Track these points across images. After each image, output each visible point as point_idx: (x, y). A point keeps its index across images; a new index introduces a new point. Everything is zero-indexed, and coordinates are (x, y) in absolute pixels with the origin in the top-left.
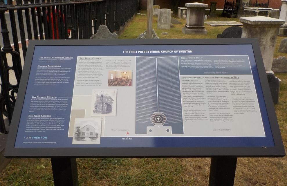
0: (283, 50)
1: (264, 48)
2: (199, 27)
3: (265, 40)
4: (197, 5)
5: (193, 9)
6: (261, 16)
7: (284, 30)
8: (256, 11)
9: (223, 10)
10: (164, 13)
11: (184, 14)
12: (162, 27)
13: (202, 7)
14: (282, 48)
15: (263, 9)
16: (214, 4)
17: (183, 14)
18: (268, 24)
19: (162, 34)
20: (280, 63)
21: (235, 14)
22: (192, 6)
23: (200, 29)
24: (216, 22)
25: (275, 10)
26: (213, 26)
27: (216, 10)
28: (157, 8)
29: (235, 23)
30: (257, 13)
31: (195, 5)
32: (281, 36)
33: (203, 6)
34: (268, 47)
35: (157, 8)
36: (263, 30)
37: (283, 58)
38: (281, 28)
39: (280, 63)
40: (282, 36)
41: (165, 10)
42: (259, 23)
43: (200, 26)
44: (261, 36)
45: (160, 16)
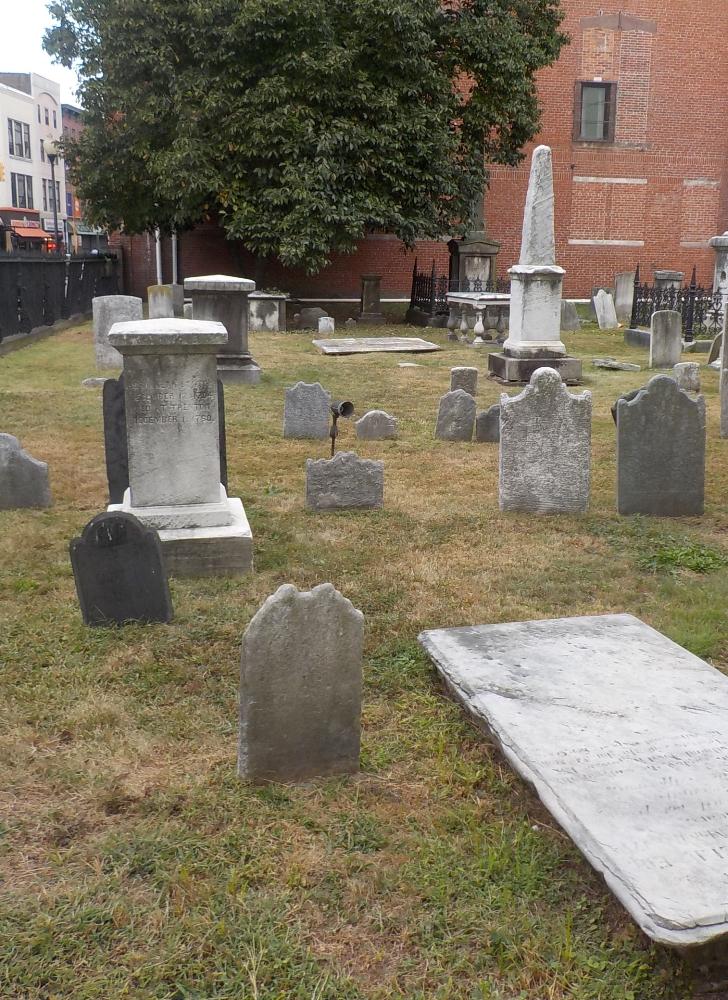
0: (451, 428)
1: (179, 426)
2: (230, 356)
3: (176, 397)
4: (216, 284)
5: (203, 297)
6: (203, 319)
7: (520, 364)
8: (475, 304)
9: (409, 300)
10: (117, 310)
11: (255, 314)
12: (111, 359)
13: (231, 289)
14: (447, 423)
15: (496, 300)
16: (373, 283)
17: (252, 315)
18: (169, 343)
19: (86, 384)
20: (341, 476)
21: (443, 316)
22: (196, 287)
23: (234, 363)
24: (352, 340)
25: (568, 301)
26: (333, 354)
27: (381, 300)
28: (162, 294)
29: (418, 343)
30: (478, 310)
31: (207, 283)
32: (512, 385)
33: (238, 286)
34: (193, 423)
35: (162, 294)
36: (160, 363)
37: (348, 459)
38: (512, 359)
39: (341, 476)
40: (515, 385)
41: (117, 301)
42: (134, 342)
43: (235, 356)
44: (155, 383)
45: (101, 322)
